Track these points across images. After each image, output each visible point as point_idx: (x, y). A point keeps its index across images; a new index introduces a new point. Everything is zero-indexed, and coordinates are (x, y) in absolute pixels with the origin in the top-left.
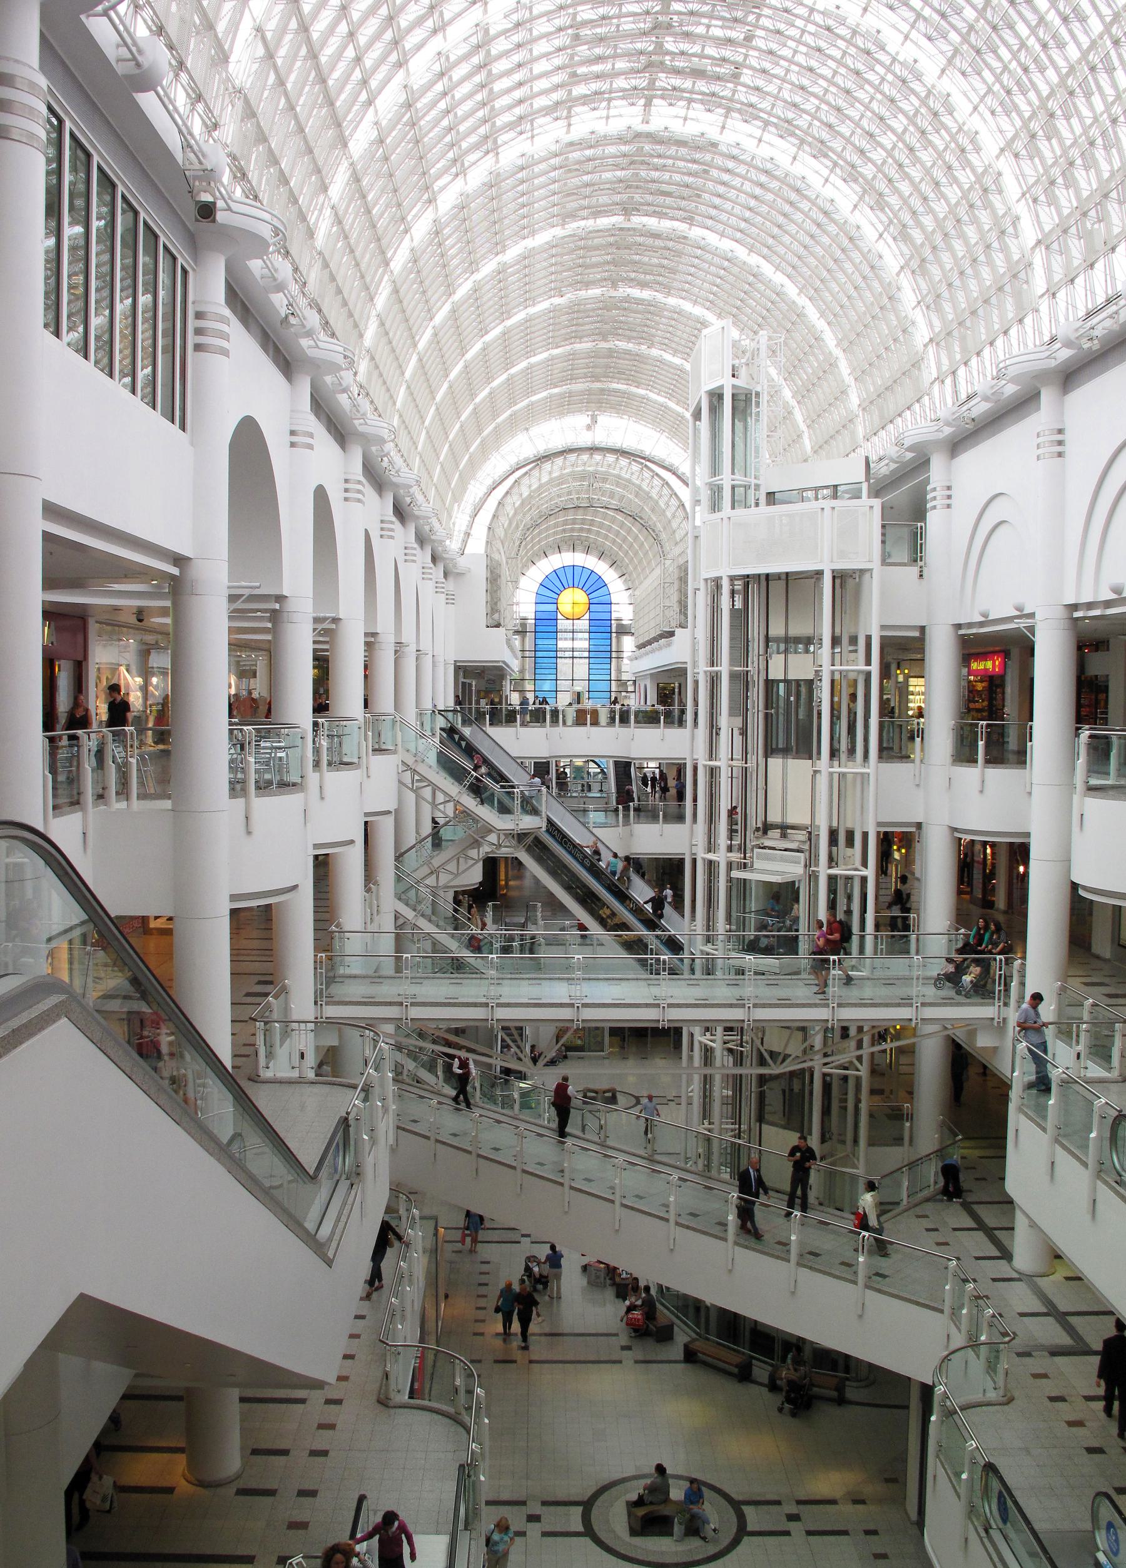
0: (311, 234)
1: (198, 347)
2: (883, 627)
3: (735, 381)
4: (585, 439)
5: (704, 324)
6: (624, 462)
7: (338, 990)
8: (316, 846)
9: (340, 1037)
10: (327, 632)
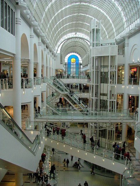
0: (33, 6)
1: (16, 23)
2: (118, 64)
3: (96, 28)
4: (75, 36)
5: (92, 19)
6: (80, 39)
8: (34, 96)
9: (38, 123)
10: (36, 64)
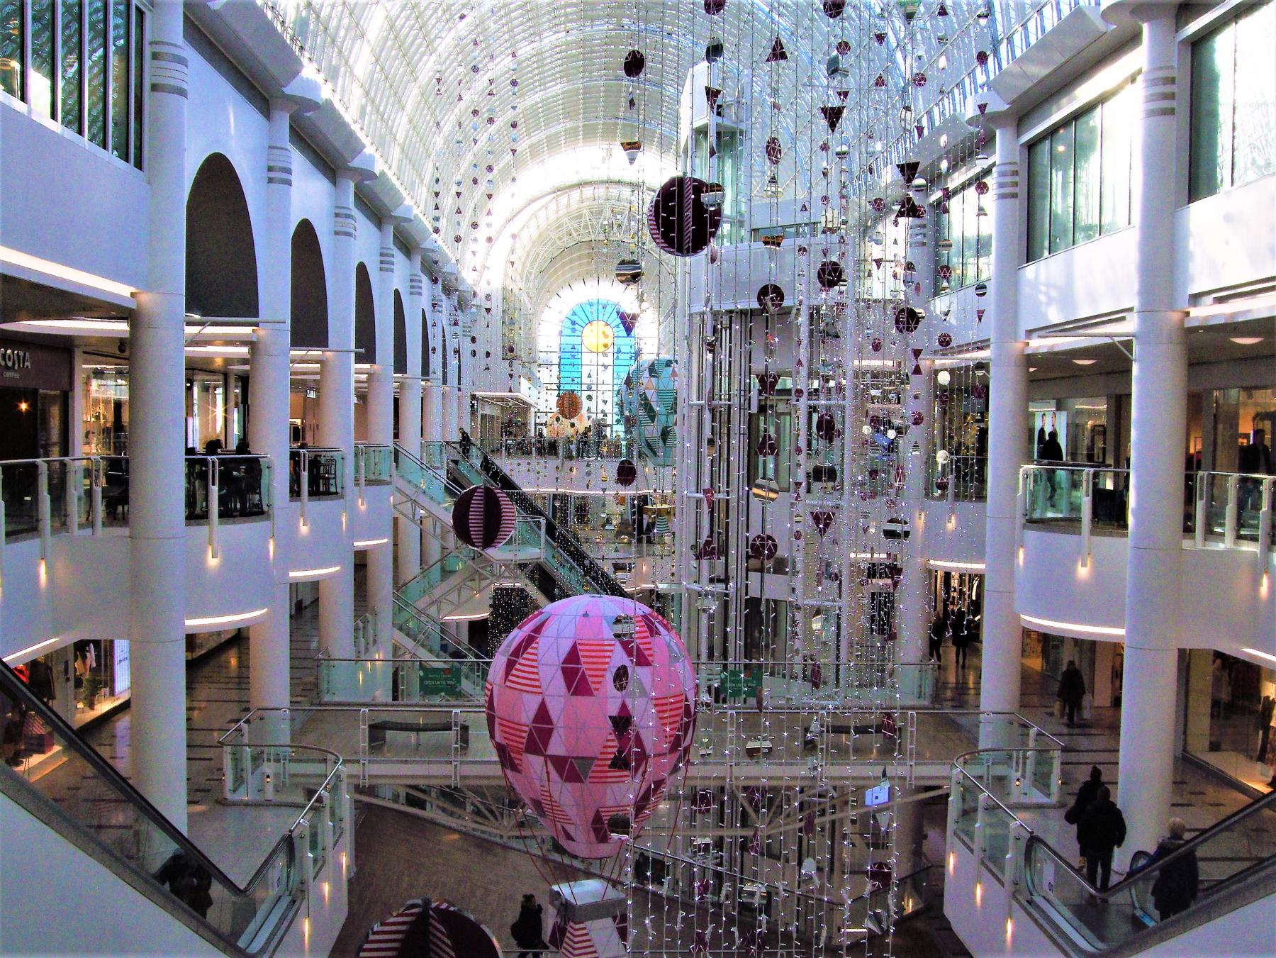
1: (155, 56)
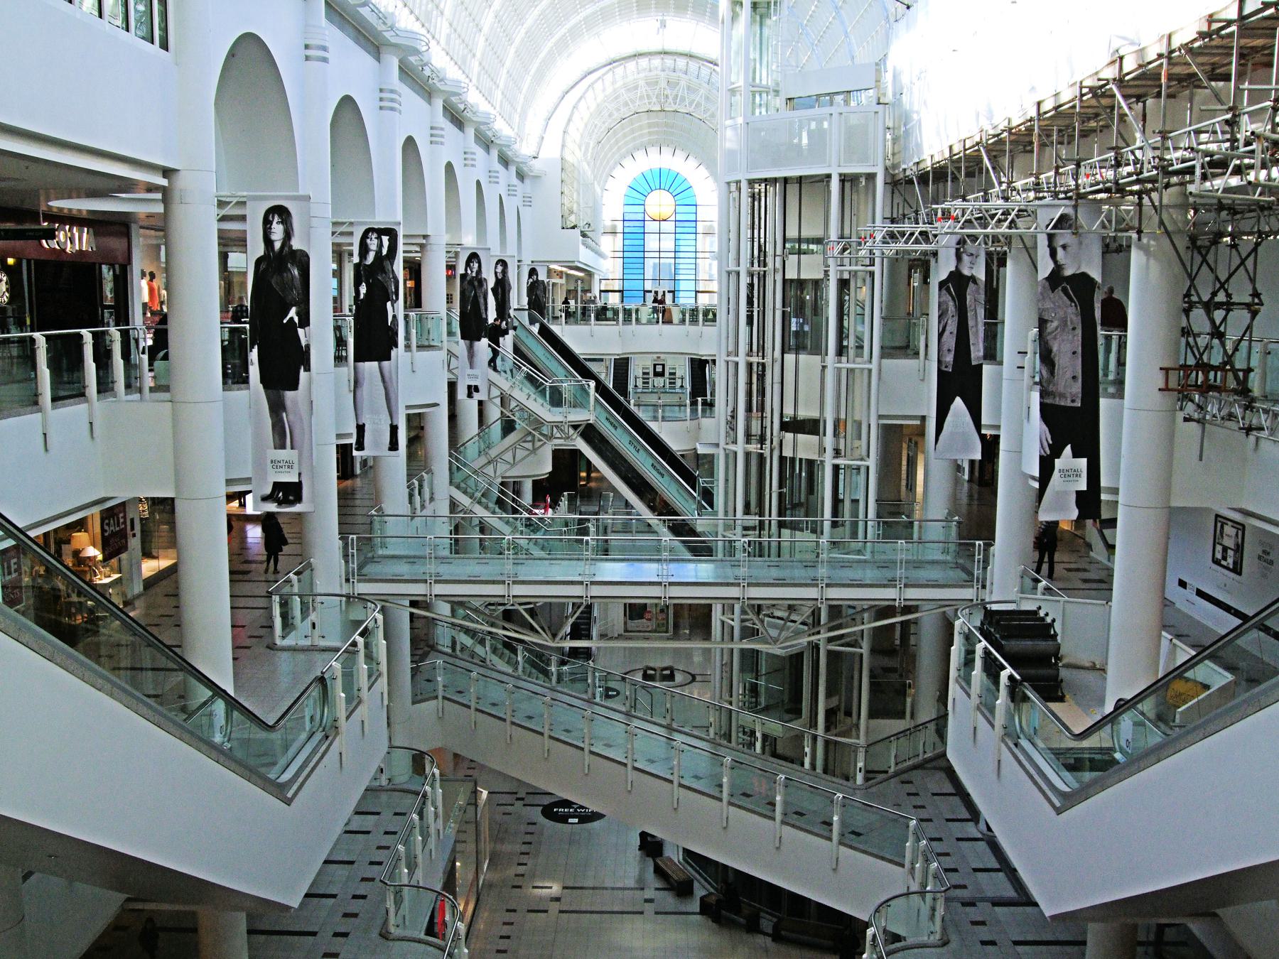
7: (370, 569)
